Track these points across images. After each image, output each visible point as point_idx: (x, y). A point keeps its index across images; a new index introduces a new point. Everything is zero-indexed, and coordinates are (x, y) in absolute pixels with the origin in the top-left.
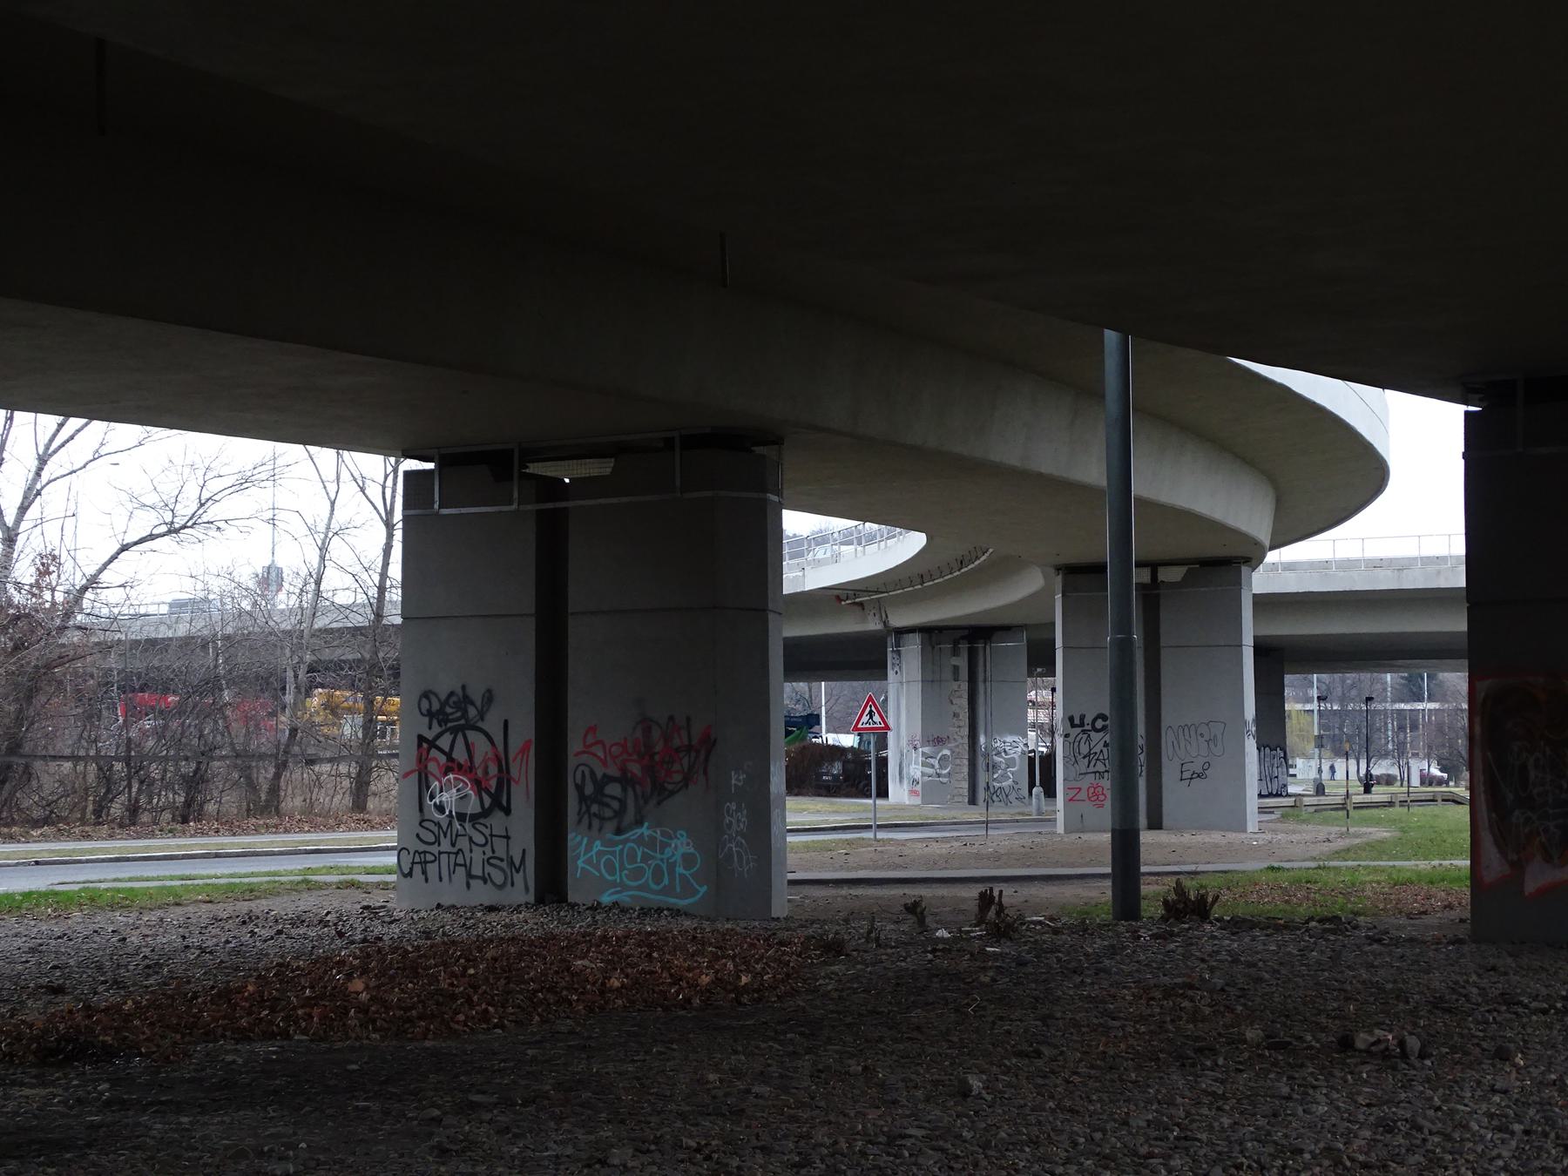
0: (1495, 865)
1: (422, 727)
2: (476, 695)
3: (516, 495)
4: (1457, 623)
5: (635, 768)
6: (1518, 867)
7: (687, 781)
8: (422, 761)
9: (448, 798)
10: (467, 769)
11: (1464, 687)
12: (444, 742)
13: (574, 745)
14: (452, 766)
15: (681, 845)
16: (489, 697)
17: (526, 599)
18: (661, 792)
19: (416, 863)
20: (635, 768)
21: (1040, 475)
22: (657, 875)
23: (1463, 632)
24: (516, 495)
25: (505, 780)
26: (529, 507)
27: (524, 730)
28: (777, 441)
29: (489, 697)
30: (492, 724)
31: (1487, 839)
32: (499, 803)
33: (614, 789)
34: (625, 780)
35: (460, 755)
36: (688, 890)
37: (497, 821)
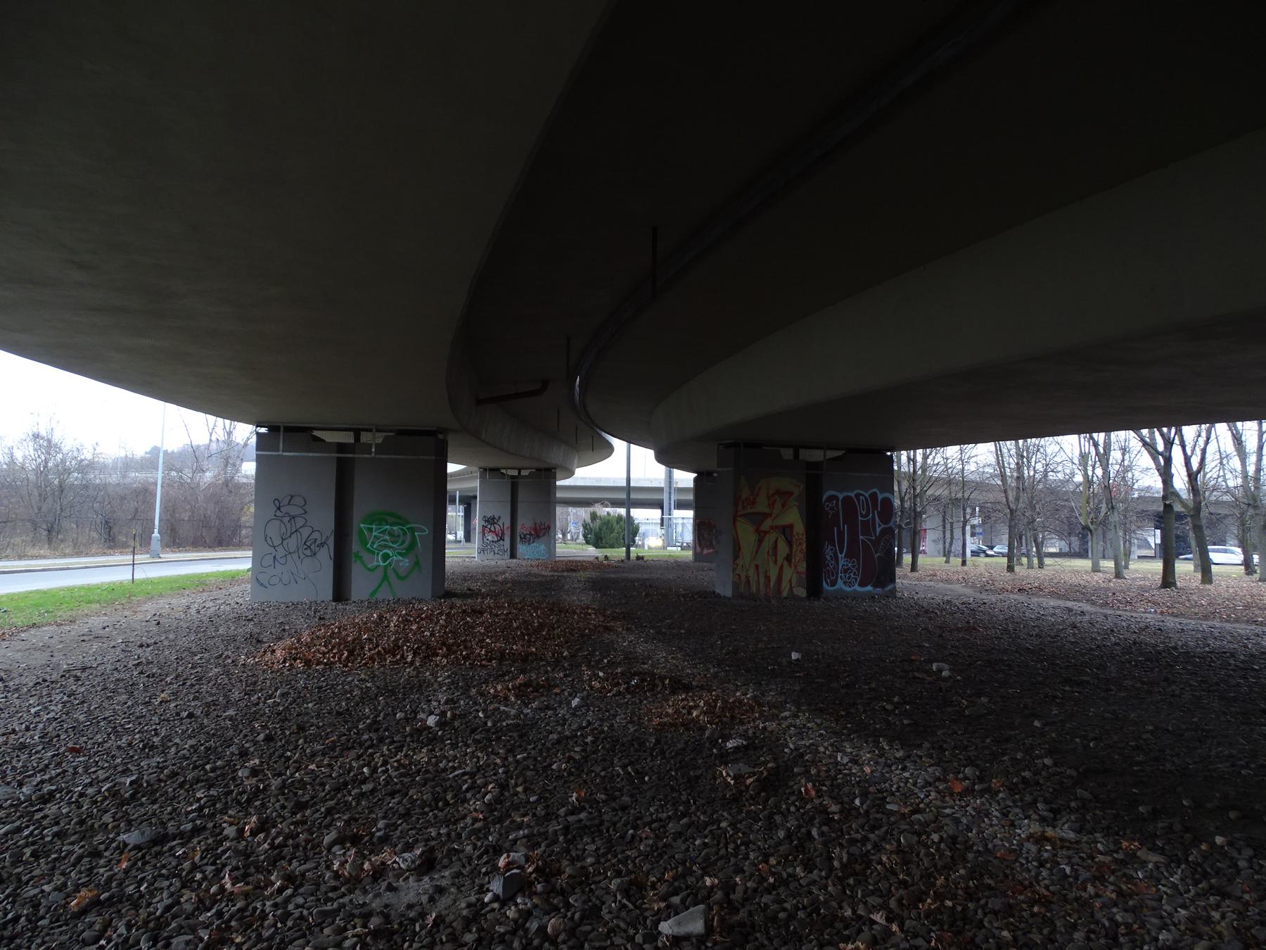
0: (698, 549)
1: (483, 523)
2: (496, 517)
3: (281, 445)
4: (691, 497)
5: (533, 532)
6: (702, 550)
7: (544, 534)
8: (483, 531)
9: (490, 538)
10: (495, 532)
11: (1200, 577)
12: (489, 526)
13: (519, 528)
14: (490, 531)
15: (543, 547)
16: (500, 518)
17: (509, 498)
18: (538, 537)
19: (482, 551)
20: (533, 532)
21: (1164, 570)
22: (537, 553)
23: (453, 462)
24: (281, 445)
25: (503, 533)
26: (334, 455)
27: (508, 524)
28: (555, 468)
29: (500, 518)
30: (500, 523)
31: (697, 545)
32: (502, 539)
33: (528, 536)
34: (530, 534)
35: (492, 529)
36: (544, 556)
37: (501, 542)
